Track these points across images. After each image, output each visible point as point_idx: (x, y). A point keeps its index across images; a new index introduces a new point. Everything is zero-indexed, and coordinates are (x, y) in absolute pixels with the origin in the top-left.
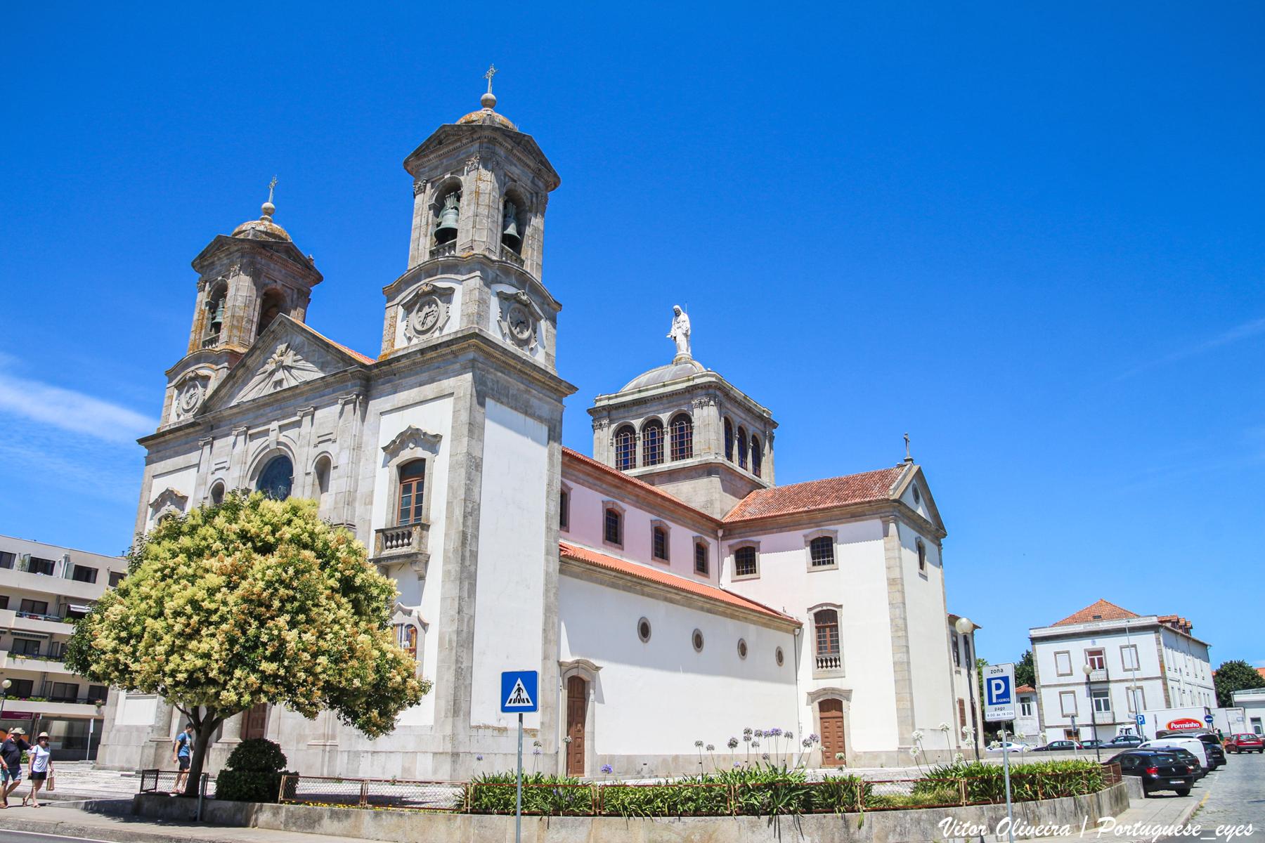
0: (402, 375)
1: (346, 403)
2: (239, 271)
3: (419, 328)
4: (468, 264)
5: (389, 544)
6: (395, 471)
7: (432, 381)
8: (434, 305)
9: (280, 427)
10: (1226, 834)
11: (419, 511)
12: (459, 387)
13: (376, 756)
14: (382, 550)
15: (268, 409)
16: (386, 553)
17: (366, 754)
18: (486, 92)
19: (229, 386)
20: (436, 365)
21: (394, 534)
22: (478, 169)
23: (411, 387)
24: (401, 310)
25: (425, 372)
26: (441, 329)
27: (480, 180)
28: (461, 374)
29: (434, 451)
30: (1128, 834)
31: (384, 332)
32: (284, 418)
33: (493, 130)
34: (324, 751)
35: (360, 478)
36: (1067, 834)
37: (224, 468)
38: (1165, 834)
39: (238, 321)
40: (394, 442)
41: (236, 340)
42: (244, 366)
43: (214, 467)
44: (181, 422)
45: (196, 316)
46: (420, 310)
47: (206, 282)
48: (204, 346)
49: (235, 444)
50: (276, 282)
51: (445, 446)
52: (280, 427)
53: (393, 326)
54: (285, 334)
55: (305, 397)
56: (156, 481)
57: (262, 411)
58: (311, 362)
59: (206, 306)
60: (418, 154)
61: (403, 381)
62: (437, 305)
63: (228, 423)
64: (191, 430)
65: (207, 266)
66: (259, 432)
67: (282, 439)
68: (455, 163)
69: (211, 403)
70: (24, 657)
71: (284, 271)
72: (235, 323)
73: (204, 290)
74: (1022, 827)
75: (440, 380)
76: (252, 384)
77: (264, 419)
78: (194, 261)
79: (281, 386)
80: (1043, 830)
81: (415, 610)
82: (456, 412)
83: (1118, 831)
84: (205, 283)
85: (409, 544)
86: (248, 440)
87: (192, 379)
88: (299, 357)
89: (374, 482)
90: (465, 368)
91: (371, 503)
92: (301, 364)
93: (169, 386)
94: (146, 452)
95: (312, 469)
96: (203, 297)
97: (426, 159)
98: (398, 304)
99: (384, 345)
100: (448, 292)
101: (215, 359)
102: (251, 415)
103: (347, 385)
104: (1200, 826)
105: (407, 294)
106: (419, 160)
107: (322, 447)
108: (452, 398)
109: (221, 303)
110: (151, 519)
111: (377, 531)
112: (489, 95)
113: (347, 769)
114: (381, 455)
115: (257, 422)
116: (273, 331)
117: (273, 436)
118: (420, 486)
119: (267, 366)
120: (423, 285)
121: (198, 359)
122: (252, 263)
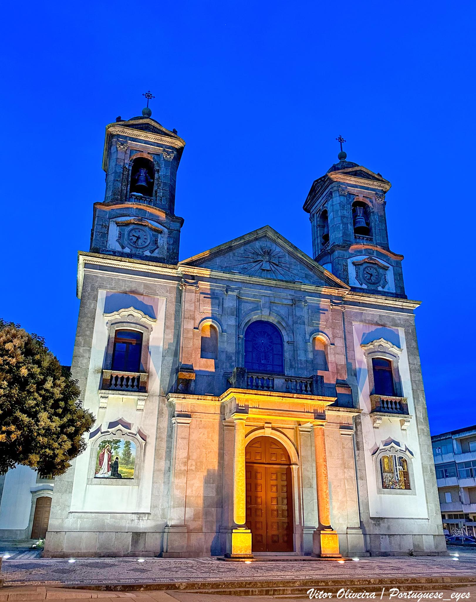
10: (456, 597)
17: (384, 536)
36: (374, 597)
70: (426, 407)
82: (277, 378)
83: (400, 596)
109: (26, 553)
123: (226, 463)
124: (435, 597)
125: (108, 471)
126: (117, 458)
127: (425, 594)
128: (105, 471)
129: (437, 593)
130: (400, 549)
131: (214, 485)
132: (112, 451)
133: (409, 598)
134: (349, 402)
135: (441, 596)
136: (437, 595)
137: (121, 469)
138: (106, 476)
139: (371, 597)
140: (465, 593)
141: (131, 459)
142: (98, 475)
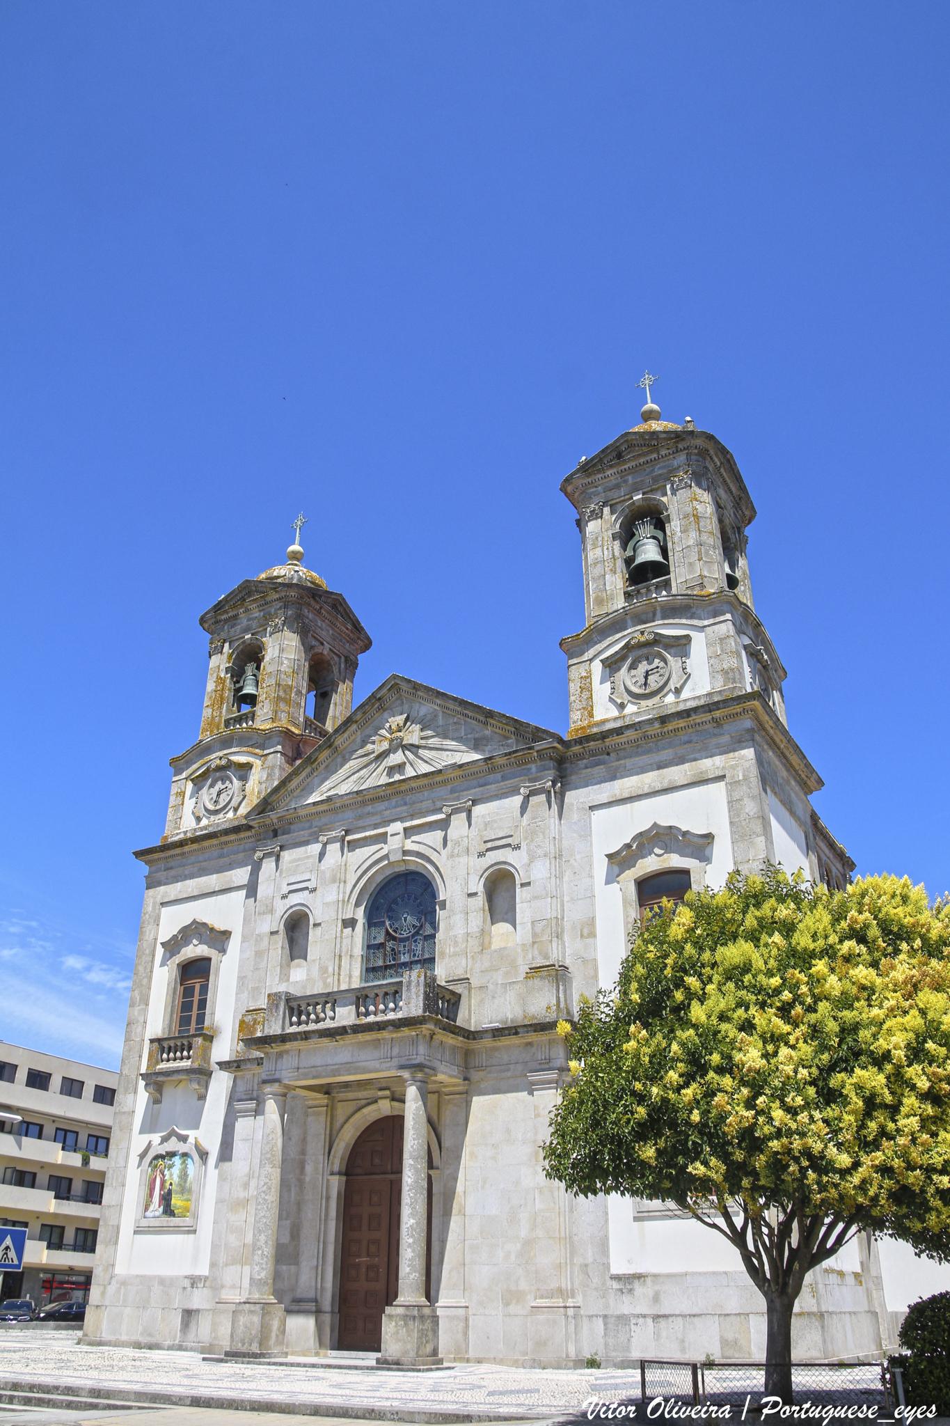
0: (622, 754)
1: (533, 793)
2: (283, 626)
3: (211, 807)
4: (710, 605)
5: (165, 1056)
6: (632, 889)
7: (681, 760)
8: (228, 782)
9: (405, 829)
10: (824, 1416)
11: (201, 1019)
12: (733, 767)
13: (663, 1323)
14: (157, 1063)
15: (380, 806)
16: (163, 1066)
17: (641, 1321)
18: (294, 544)
19: (304, 774)
20: (686, 738)
21: (179, 1044)
22: (691, 486)
23: (643, 770)
24: (190, 785)
25: (664, 749)
26: (678, 691)
27: (696, 500)
28: (734, 750)
29: (705, 858)
30: (796, 1416)
31: (572, 698)
32: (412, 816)
33: (707, 438)
34: (566, 1316)
35: (566, 899)
36: (727, 1416)
37: (307, 888)
38: (837, 1416)
39: (285, 691)
40: (628, 846)
41: (283, 716)
42: (330, 746)
43: (285, 889)
44: (201, 829)
45: (211, 686)
46: (212, 786)
47: (225, 641)
48: (227, 725)
49: (322, 855)
50: (322, 644)
51: (234, 944)
52: (405, 829)
53: (587, 688)
54: (399, 702)
55: (449, 787)
56: (165, 911)
57: (369, 808)
58: (453, 739)
59: (227, 673)
60: (587, 469)
61: (628, 762)
62: (231, 782)
63: (307, 825)
64: (232, 837)
65: (226, 621)
66: (365, 838)
67: (409, 845)
68: (648, 480)
69: (274, 798)
71: (331, 632)
72: (281, 693)
73: (221, 653)
74: (677, 1408)
75: (695, 760)
76: (343, 772)
77: (377, 819)
78: (206, 614)
79: (402, 773)
80: (700, 1411)
81: (192, 1134)
83: (784, 1413)
84: (224, 643)
85: (188, 1058)
86: (346, 849)
87: (219, 768)
88: (430, 733)
89: (593, 905)
90: (740, 742)
91: (593, 935)
92: (434, 742)
93: (175, 779)
94: (145, 869)
95: (478, 887)
96: (220, 663)
97: (599, 476)
98: (186, 778)
99: (575, 716)
100: (684, 641)
101: (260, 741)
102: (349, 814)
103: (529, 769)
104: (876, 1407)
105: (197, 768)
106: (588, 477)
107: (295, 899)
108: (722, 784)
110: (163, 964)
111: (152, 1041)
112: (296, 547)
113: (606, 1345)
114: (160, 951)
115: (361, 823)
116: (380, 699)
117: (394, 843)
118: (204, 989)
119: (370, 747)
120: (215, 759)
121: (226, 742)
122: (299, 617)
123: (307, 1179)
124: (861, 1416)
125: (159, 1206)
126: (171, 1184)
127: (840, 1408)
128: (156, 1207)
129: (865, 1407)
130: (683, 1350)
131: (288, 1222)
132: (166, 1172)
133: (803, 1416)
134: (549, 1008)
135: (872, 1414)
136: (865, 1411)
137: (176, 1201)
138: (157, 1214)
139: (721, 1416)
140: (925, 1407)
141: (188, 1184)
142: (148, 1214)
